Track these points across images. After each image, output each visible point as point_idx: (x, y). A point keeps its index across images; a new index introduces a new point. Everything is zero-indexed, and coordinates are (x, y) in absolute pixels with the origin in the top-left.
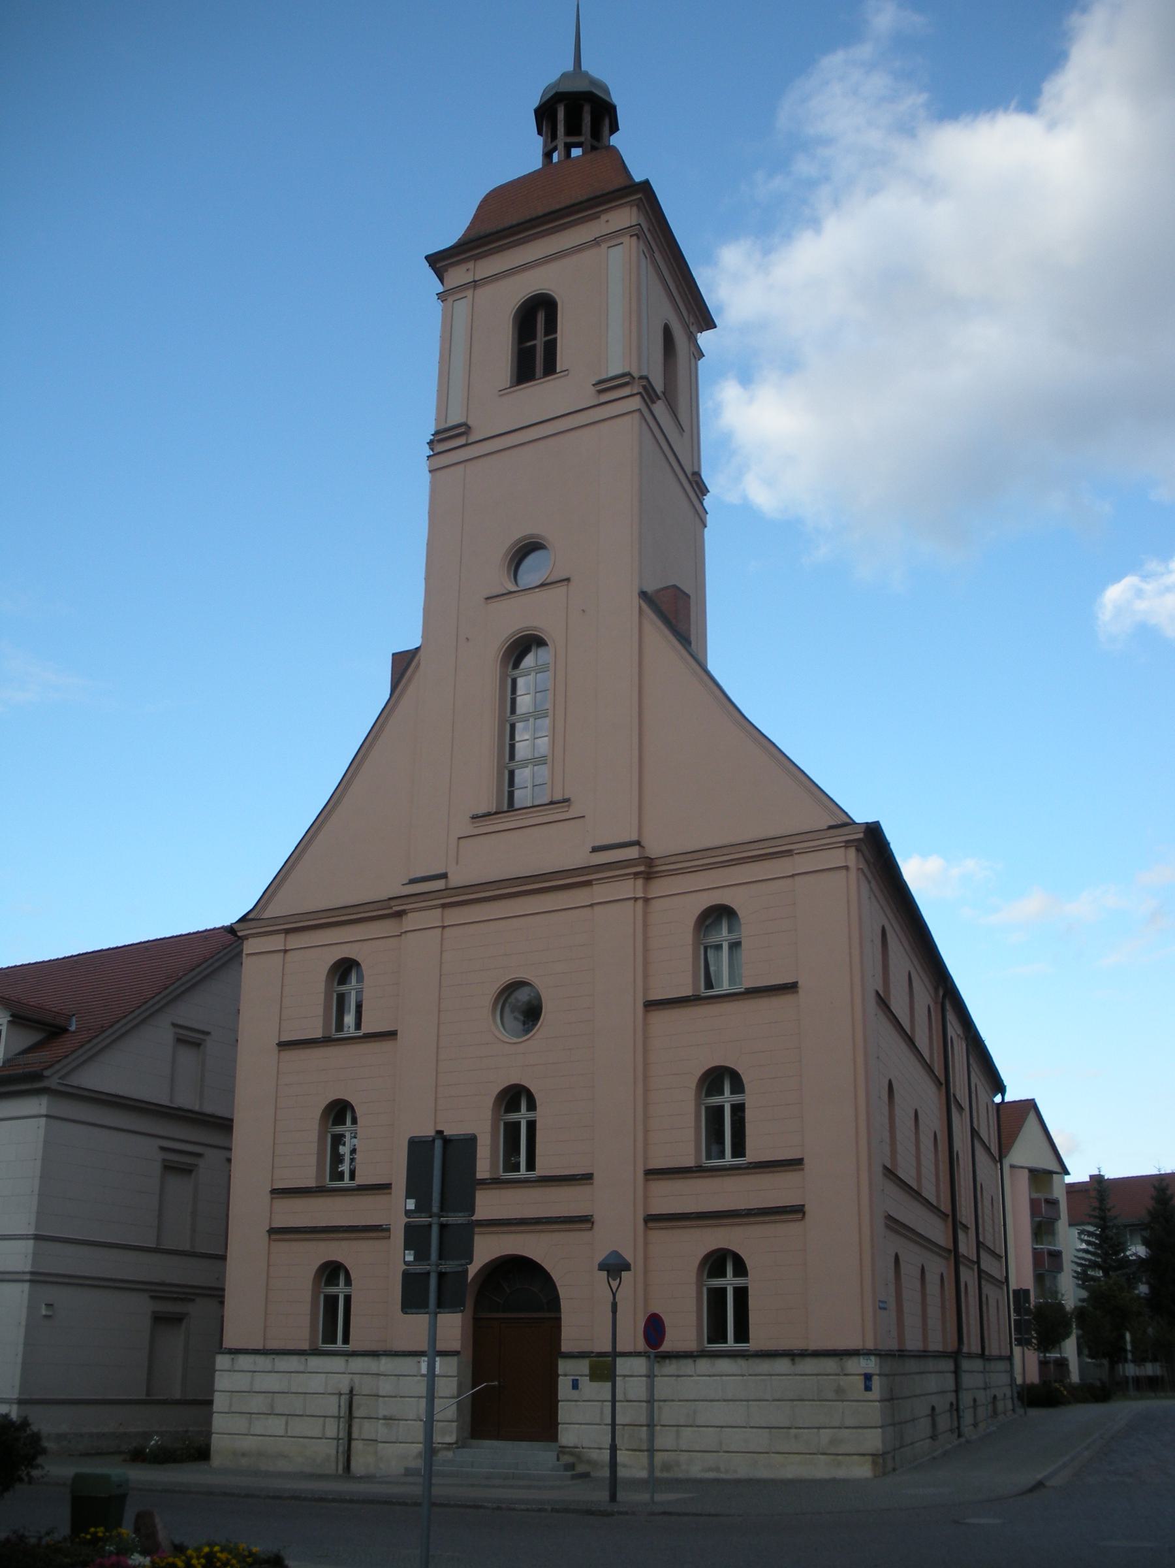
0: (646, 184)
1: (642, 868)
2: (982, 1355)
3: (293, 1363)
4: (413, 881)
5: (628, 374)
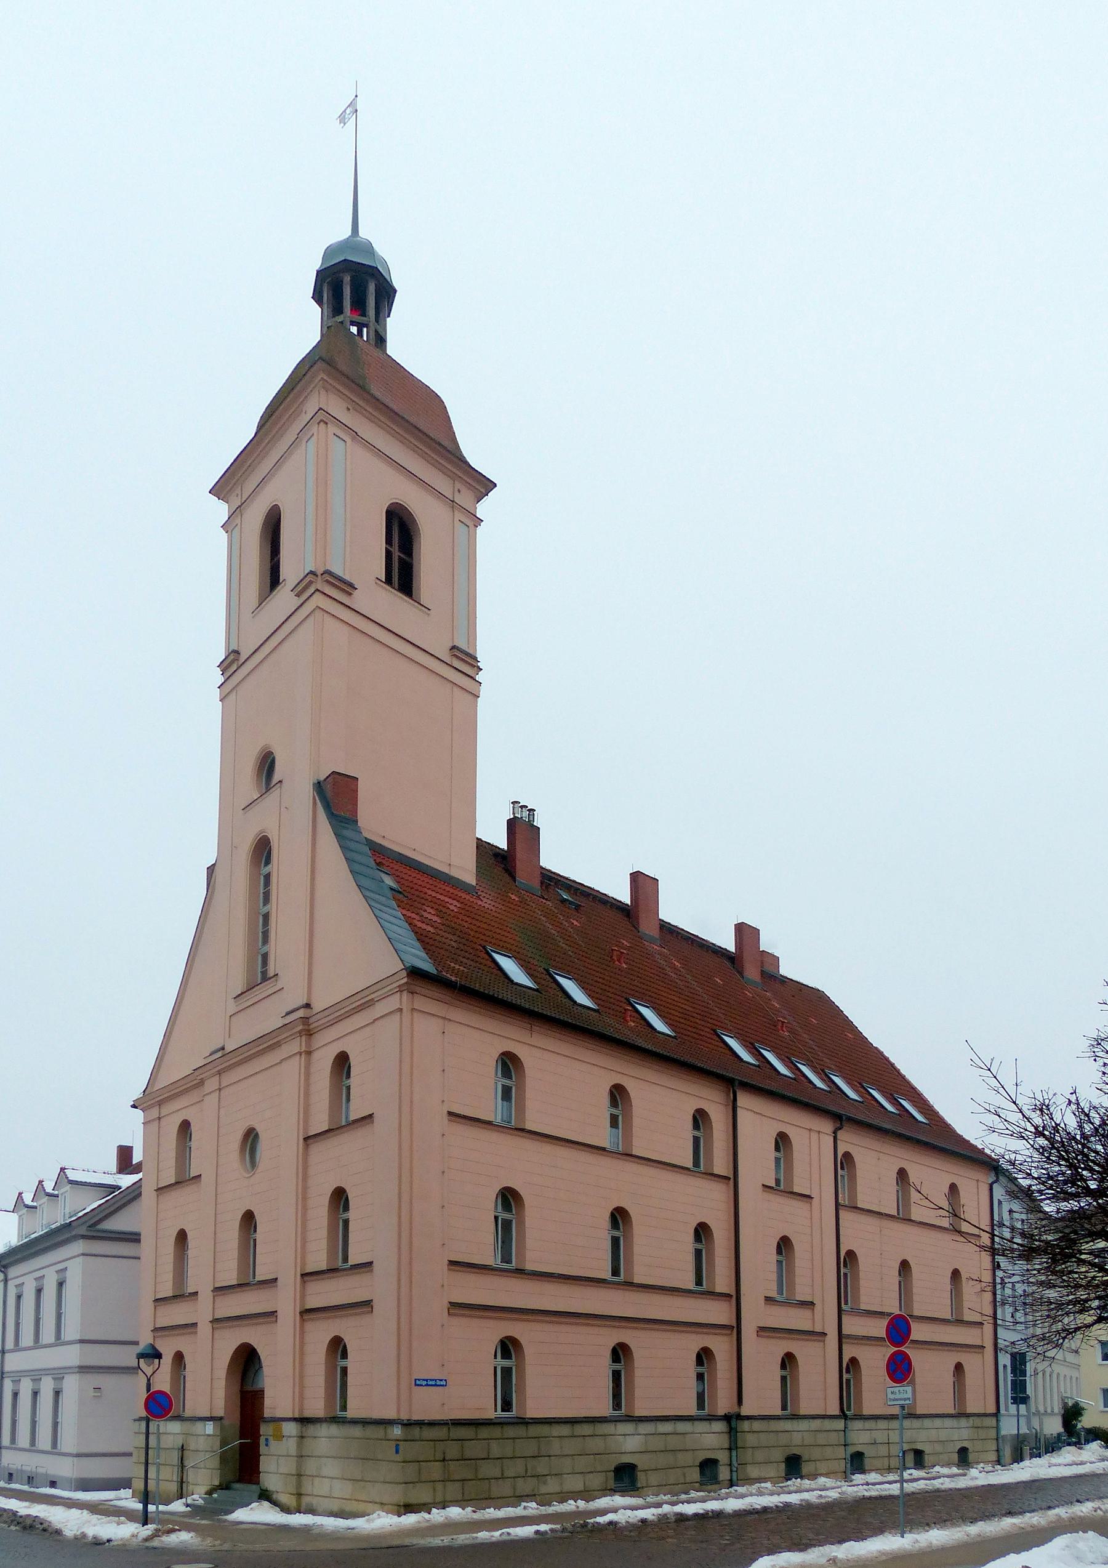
0: (220, 490)
1: (301, 1027)
2: (843, 1416)
3: (948, 1422)
4: (288, 1014)
5: (311, 572)
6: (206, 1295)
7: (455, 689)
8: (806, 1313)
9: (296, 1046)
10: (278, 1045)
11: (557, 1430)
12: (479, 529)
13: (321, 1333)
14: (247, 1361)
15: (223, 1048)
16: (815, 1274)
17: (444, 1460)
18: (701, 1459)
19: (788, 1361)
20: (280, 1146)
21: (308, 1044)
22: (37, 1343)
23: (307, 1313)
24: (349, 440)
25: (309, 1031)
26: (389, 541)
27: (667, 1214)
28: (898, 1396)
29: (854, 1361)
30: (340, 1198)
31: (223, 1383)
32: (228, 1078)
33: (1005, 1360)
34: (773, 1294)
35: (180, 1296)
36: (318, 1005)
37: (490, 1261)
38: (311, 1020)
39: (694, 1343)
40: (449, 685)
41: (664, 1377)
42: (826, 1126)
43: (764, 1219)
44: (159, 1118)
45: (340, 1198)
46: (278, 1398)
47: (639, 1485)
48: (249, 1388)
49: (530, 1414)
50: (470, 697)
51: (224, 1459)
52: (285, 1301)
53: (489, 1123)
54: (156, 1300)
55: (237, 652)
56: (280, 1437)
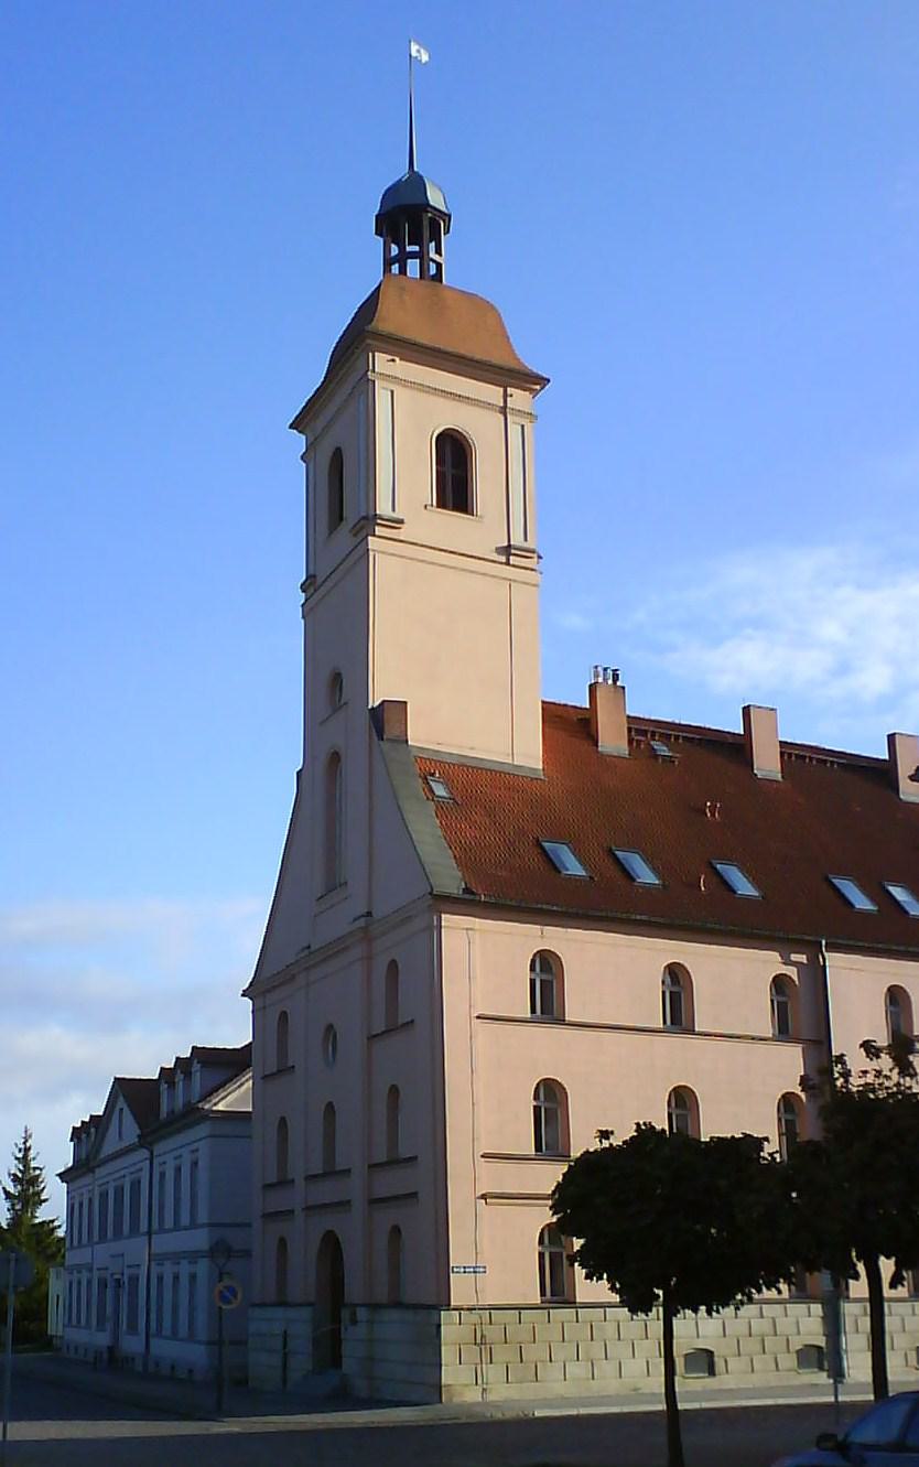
0: (297, 424)
6: (300, 1182)
10: (346, 949)
13: (387, 1217)
14: (331, 1246)
15: (309, 947)
22: (177, 1227)
23: (375, 1202)
35: (331, 1173)
36: (377, 914)
44: (265, 1008)
55: (314, 576)
56: (354, 1322)
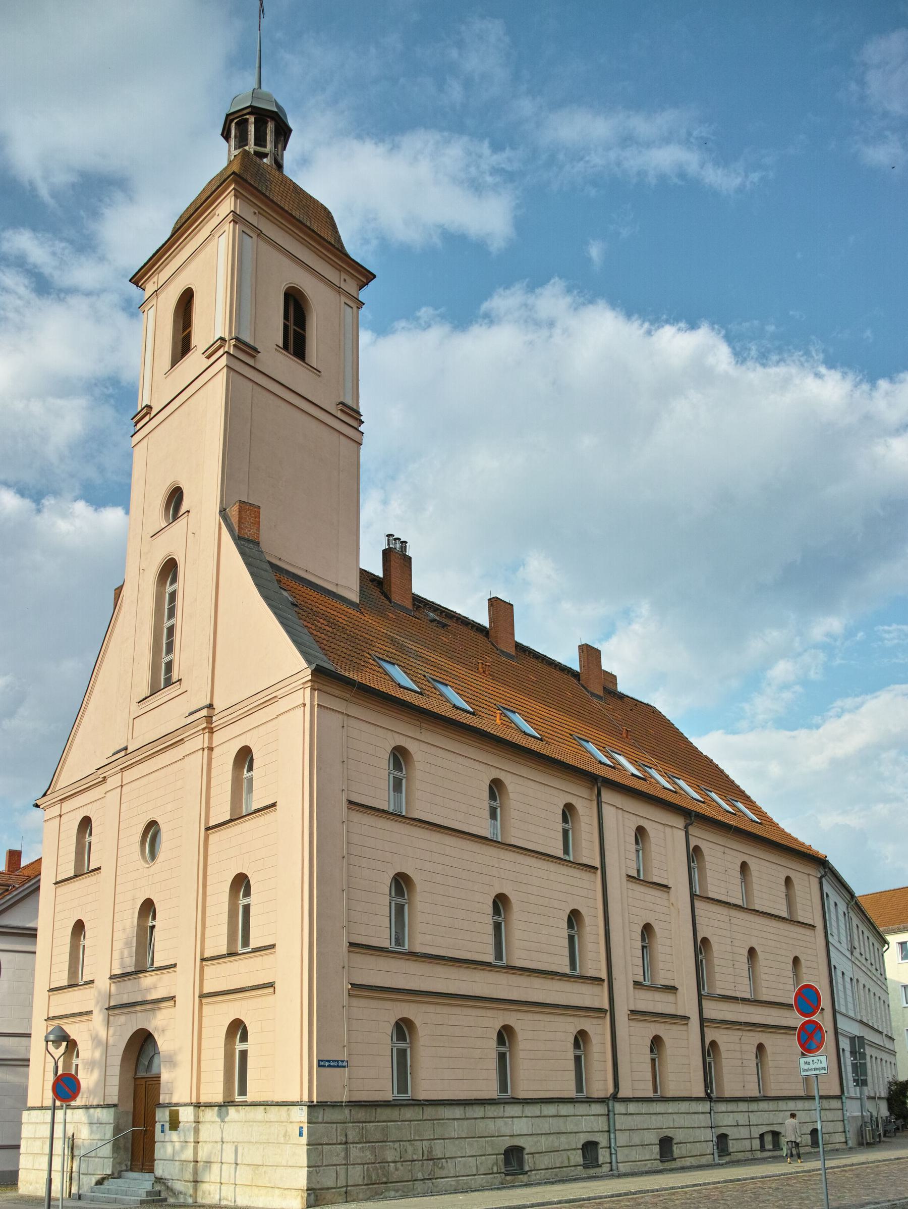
1: (204, 725)
2: (709, 1098)
4: (191, 714)
7: (341, 437)
8: (670, 997)
9: (200, 741)
11: (447, 1112)
12: (361, 311)
14: (142, 1045)
15: (126, 749)
16: (675, 961)
17: (346, 1143)
18: (582, 1142)
19: (657, 1043)
20: (181, 838)
21: (211, 740)
24: (254, 236)
25: (212, 728)
26: (286, 317)
27: (544, 899)
28: (812, 1066)
29: (713, 1044)
30: (241, 883)
31: (117, 1070)
32: (129, 775)
33: (845, 1044)
34: (641, 979)
36: (219, 705)
37: (386, 944)
38: (214, 719)
39: (570, 1026)
40: (336, 434)
41: (544, 1061)
42: (680, 822)
43: (631, 907)
45: (241, 883)
46: (177, 1084)
47: (527, 1168)
48: (141, 1074)
49: (422, 1096)
50: (355, 445)
51: (116, 1147)
52: (181, 984)
53: (384, 811)
54: (51, 990)
